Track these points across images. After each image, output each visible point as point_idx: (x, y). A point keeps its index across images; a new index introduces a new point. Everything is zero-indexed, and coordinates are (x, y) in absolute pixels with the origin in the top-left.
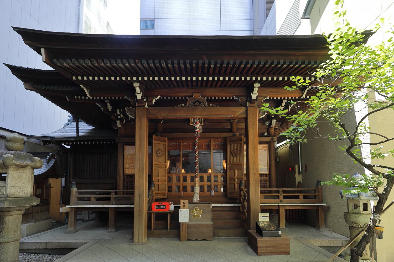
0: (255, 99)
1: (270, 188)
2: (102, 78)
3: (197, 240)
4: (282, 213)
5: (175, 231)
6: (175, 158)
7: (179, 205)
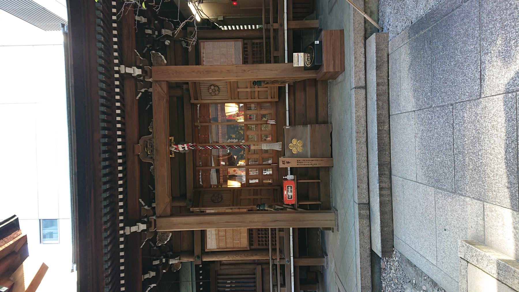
0: (140, 70)
1: (263, 38)
2: (122, 275)
3: (331, 145)
4: (296, 25)
5: (322, 174)
6: (221, 178)
7: (289, 169)
